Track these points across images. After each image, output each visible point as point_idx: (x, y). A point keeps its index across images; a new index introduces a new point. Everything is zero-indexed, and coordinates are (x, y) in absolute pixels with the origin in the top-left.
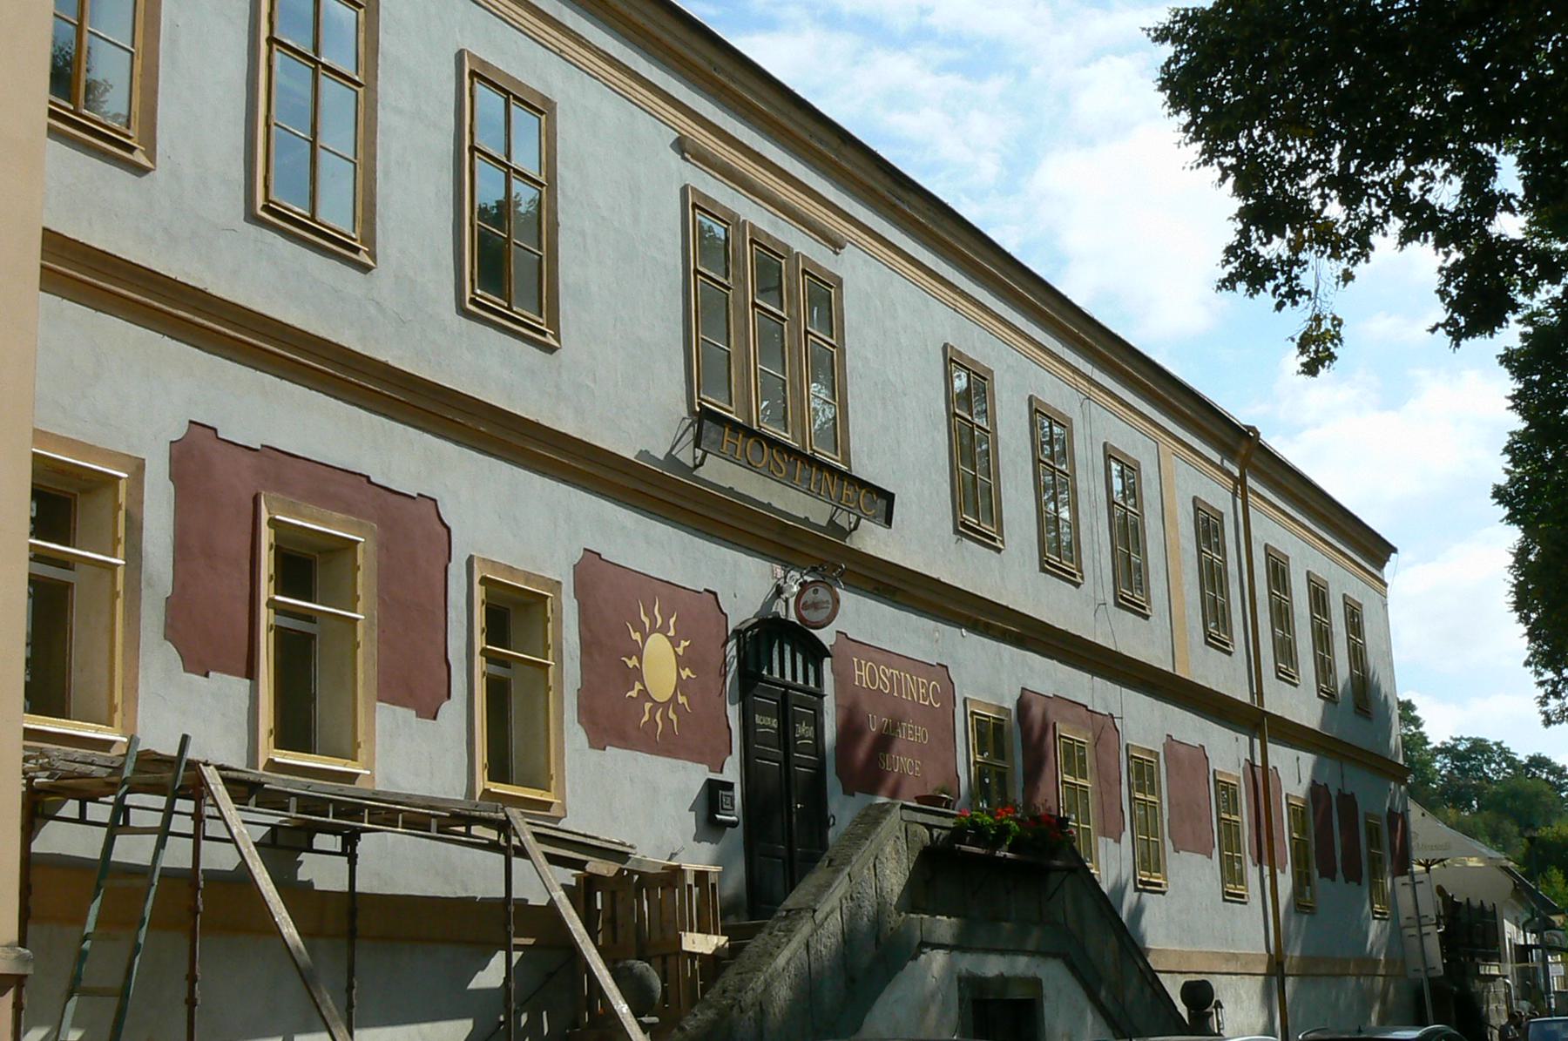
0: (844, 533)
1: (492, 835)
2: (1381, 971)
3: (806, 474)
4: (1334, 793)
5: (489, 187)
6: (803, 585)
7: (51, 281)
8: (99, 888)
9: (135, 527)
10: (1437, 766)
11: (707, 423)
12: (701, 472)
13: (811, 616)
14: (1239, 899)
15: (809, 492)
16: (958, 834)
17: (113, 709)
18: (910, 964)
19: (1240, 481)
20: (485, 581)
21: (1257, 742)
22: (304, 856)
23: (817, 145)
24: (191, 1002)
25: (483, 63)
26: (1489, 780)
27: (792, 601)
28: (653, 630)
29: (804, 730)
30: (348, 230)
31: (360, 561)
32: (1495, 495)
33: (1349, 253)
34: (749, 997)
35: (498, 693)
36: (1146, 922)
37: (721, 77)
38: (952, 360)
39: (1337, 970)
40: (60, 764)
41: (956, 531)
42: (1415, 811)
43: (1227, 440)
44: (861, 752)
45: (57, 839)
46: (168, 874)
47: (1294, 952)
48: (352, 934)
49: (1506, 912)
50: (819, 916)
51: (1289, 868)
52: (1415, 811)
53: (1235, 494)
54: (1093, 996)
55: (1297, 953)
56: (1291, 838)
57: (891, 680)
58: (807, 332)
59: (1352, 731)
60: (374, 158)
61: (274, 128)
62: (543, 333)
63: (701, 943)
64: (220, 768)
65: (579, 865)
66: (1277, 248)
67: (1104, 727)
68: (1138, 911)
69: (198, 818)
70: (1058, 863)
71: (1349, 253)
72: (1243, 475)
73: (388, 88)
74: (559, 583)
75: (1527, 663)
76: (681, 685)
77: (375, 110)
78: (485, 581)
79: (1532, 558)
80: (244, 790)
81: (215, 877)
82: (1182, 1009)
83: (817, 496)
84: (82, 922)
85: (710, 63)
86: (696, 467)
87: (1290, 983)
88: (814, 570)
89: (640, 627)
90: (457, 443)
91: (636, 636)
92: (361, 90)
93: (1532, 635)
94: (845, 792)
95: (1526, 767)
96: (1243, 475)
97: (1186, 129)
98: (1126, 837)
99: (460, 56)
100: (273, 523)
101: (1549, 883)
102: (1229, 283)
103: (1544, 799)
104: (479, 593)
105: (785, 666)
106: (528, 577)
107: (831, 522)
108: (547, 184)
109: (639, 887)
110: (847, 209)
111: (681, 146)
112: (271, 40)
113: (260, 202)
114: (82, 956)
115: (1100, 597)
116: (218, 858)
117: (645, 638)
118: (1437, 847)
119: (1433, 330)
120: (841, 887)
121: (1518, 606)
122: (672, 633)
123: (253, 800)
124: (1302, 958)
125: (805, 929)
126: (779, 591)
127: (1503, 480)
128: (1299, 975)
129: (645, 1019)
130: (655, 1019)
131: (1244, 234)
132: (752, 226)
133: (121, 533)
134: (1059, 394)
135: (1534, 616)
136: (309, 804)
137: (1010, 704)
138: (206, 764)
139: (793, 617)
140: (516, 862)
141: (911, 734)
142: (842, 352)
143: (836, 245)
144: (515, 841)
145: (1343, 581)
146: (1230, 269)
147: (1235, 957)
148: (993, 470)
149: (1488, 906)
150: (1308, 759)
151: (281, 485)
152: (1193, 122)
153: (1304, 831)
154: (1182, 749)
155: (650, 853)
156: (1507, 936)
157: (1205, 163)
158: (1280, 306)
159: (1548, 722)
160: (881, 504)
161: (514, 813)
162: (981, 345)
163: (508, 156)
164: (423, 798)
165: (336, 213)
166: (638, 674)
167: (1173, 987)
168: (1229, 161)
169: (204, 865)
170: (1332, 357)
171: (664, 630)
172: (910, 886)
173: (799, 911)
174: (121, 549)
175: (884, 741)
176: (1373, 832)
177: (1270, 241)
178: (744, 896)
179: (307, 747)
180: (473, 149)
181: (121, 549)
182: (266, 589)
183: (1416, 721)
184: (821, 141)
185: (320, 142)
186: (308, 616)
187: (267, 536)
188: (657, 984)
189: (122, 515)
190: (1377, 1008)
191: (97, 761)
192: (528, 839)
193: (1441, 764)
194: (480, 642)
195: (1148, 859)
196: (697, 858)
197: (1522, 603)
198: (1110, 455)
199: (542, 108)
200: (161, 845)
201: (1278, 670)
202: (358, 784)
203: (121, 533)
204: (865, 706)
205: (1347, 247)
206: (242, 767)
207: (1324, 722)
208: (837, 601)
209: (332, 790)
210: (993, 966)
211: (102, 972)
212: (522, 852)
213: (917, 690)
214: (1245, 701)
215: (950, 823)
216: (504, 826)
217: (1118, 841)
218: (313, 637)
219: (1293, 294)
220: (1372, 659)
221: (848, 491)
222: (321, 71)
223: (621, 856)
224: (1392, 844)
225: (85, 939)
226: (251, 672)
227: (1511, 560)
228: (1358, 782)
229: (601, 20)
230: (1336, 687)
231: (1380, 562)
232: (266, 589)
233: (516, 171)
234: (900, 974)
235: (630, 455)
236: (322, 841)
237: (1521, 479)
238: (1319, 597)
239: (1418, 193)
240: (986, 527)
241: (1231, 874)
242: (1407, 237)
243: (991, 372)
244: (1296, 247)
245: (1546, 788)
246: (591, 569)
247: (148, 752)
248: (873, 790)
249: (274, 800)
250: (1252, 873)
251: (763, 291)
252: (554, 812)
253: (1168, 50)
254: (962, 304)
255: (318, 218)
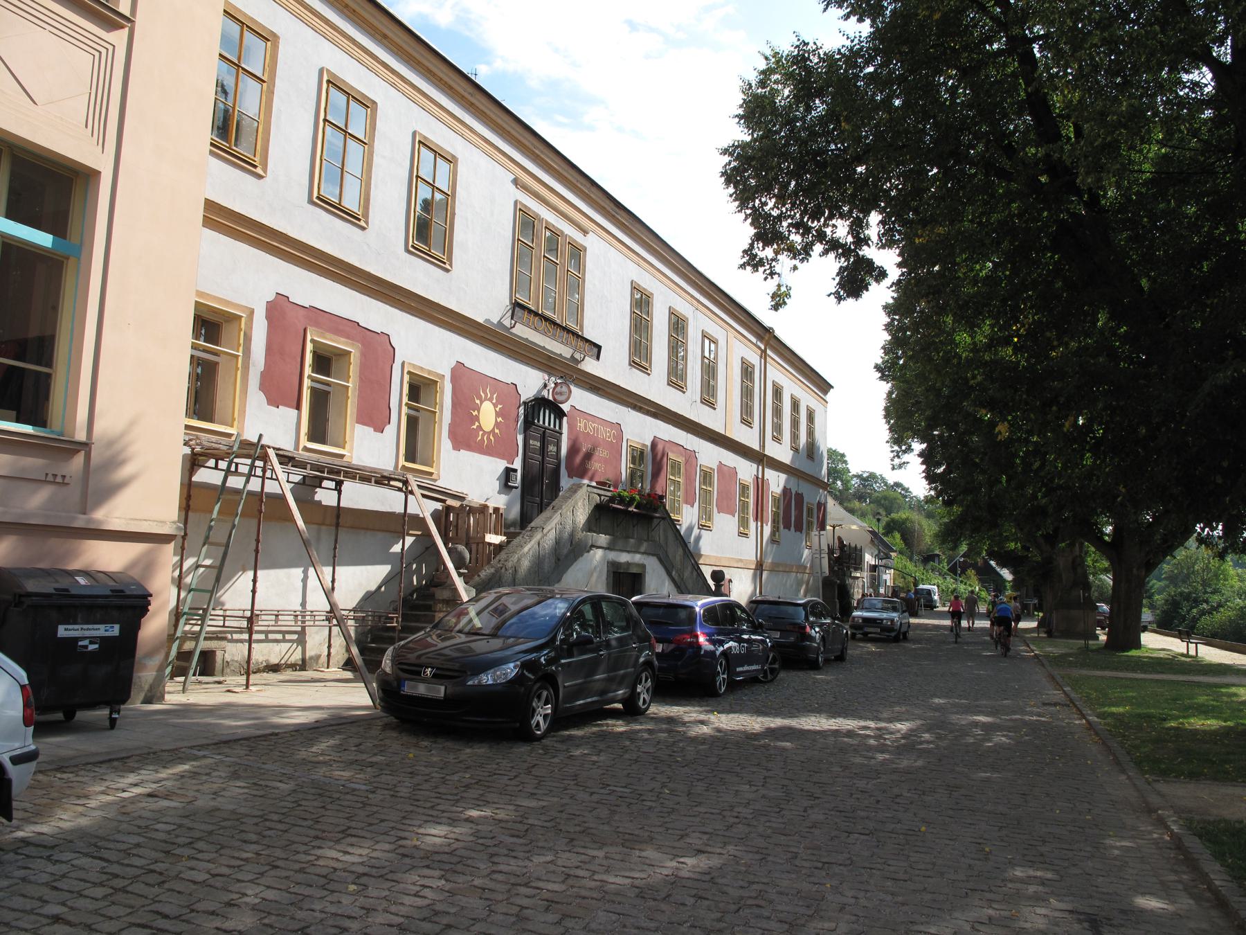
0: (578, 362)
1: (400, 485)
2: (807, 571)
3: (562, 334)
4: (794, 493)
5: (424, 192)
6: (556, 384)
7: (208, 222)
8: (219, 499)
9: (248, 339)
10: (853, 482)
11: (517, 309)
12: (513, 331)
13: (559, 398)
14: (746, 536)
15: (562, 343)
16: (612, 499)
17: (234, 420)
18: (586, 554)
19: (764, 352)
20: (409, 373)
21: (760, 468)
22: (318, 490)
23: (579, 185)
24: (257, 551)
25: (425, 138)
26: (875, 491)
27: (551, 391)
28: (486, 399)
29: (552, 448)
30: (356, 211)
31: (352, 360)
32: (875, 367)
33: (801, 257)
34: (510, 564)
35: (412, 423)
36: (702, 543)
37: (537, 152)
38: (635, 288)
39: (787, 570)
40: (205, 443)
41: (630, 365)
42: (831, 504)
43: (759, 332)
44: (578, 459)
45: (208, 475)
46: (250, 493)
47: (769, 561)
48: (337, 525)
49: (866, 550)
50: (545, 531)
51: (769, 523)
52: (831, 504)
53: (761, 357)
54: (669, 574)
55: (770, 561)
56: (772, 511)
57: (594, 429)
58: (568, 270)
59: (805, 466)
60: (371, 178)
61: (324, 162)
62: (445, 263)
63: (494, 539)
64: (274, 448)
65: (443, 501)
66: (769, 252)
67: (691, 456)
68: (698, 538)
69: (264, 471)
70: (657, 515)
71: (801, 257)
72: (765, 349)
73: (378, 145)
74: (444, 376)
75: (887, 442)
76: (497, 424)
77: (372, 156)
78: (409, 373)
79: (894, 396)
80: (285, 459)
81: (270, 496)
82: (711, 583)
83: (566, 344)
84: (211, 512)
85: (532, 144)
86: (511, 328)
87: (765, 574)
88: (562, 377)
89: (479, 397)
90: (401, 310)
91: (478, 402)
92: (366, 146)
93: (891, 430)
94: (569, 476)
95: (892, 486)
96: (765, 349)
97: (731, 196)
98: (696, 504)
99: (414, 134)
100: (313, 341)
101: (894, 538)
102: (743, 266)
103: (898, 501)
104: (406, 378)
105: (546, 419)
106: (430, 372)
107: (572, 356)
108: (450, 196)
109: (469, 514)
110: (592, 216)
111: (516, 182)
112: (325, 120)
113: (315, 194)
114: (210, 528)
115: (694, 399)
116: (271, 487)
117: (481, 403)
118: (837, 519)
119: (829, 295)
120: (556, 518)
121: (886, 417)
122: (494, 401)
123: (290, 464)
124: (772, 563)
125: (538, 536)
126: (545, 386)
127: (879, 361)
128: (771, 571)
129: (461, 571)
130: (466, 571)
131: (752, 245)
132: (546, 221)
133: (242, 341)
134: (684, 308)
135: (892, 421)
136: (315, 467)
137: (649, 443)
138: (269, 447)
139: (551, 398)
140: (410, 497)
141: (601, 453)
142: (584, 281)
143: (585, 232)
144: (410, 488)
145: (807, 398)
146: (745, 260)
147: (741, 560)
148: (649, 338)
149: (859, 547)
150: (783, 477)
151: (317, 324)
152: (735, 192)
153: (778, 508)
154: (725, 468)
155: (475, 497)
156: (866, 560)
157: (739, 211)
158: (766, 279)
159: (893, 468)
160: (596, 350)
161: (410, 477)
162: (649, 282)
163: (434, 182)
164: (370, 467)
165: (351, 202)
166: (477, 419)
167: (707, 572)
168: (749, 212)
169: (266, 490)
170: (785, 303)
171: (491, 400)
172: (589, 521)
173: (537, 528)
174: (241, 349)
175: (589, 456)
176: (810, 511)
177: (764, 249)
178: (519, 519)
179: (323, 442)
180: (417, 177)
181: (241, 349)
182: (308, 370)
183: (845, 462)
184: (582, 184)
185: (345, 169)
186: (328, 384)
187: (309, 347)
188: (467, 556)
189: (242, 333)
190: (804, 587)
191: (223, 442)
192: (416, 489)
193: (855, 482)
194: (405, 400)
195: (706, 514)
196: (498, 501)
197: (888, 414)
198: (705, 335)
199: (451, 160)
200: (247, 481)
201: (773, 436)
202: (345, 459)
203: (242, 341)
204: (581, 439)
205: (800, 254)
206: (292, 449)
207: (792, 461)
208: (570, 391)
209: (330, 462)
210: (624, 558)
211: (219, 535)
212: (412, 492)
213: (605, 434)
214: (754, 448)
215: (609, 494)
216: (406, 483)
217: (692, 506)
218: (329, 392)
219: (772, 274)
220: (817, 435)
221: (580, 343)
222: (348, 136)
223: (462, 499)
224: (818, 517)
225: (212, 521)
226: (298, 407)
227: (885, 396)
228: (805, 489)
229: (482, 120)
230: (799, 446)
231: (826, 392)
232: (308, 370)
233: (437, 188)
234: (580, 558)
235: (481, 320)
236: (326, 483)
237: (887, 361)
238: (795, 405)
239: (830, 234)
240: (644, 363)
241: (743, 522)
242: (825, 252)
243: (652, 294)
244: (777, 253)
245: (900, 496)
246: (279, 308)
247: (246, 440)
248: (582, 476)
249: (300, 465)
250: (752, 524)
251: (550, 250)
252: (434, 477)
253: (727, 159)
254: (642, 262)
255: (342, 204)
